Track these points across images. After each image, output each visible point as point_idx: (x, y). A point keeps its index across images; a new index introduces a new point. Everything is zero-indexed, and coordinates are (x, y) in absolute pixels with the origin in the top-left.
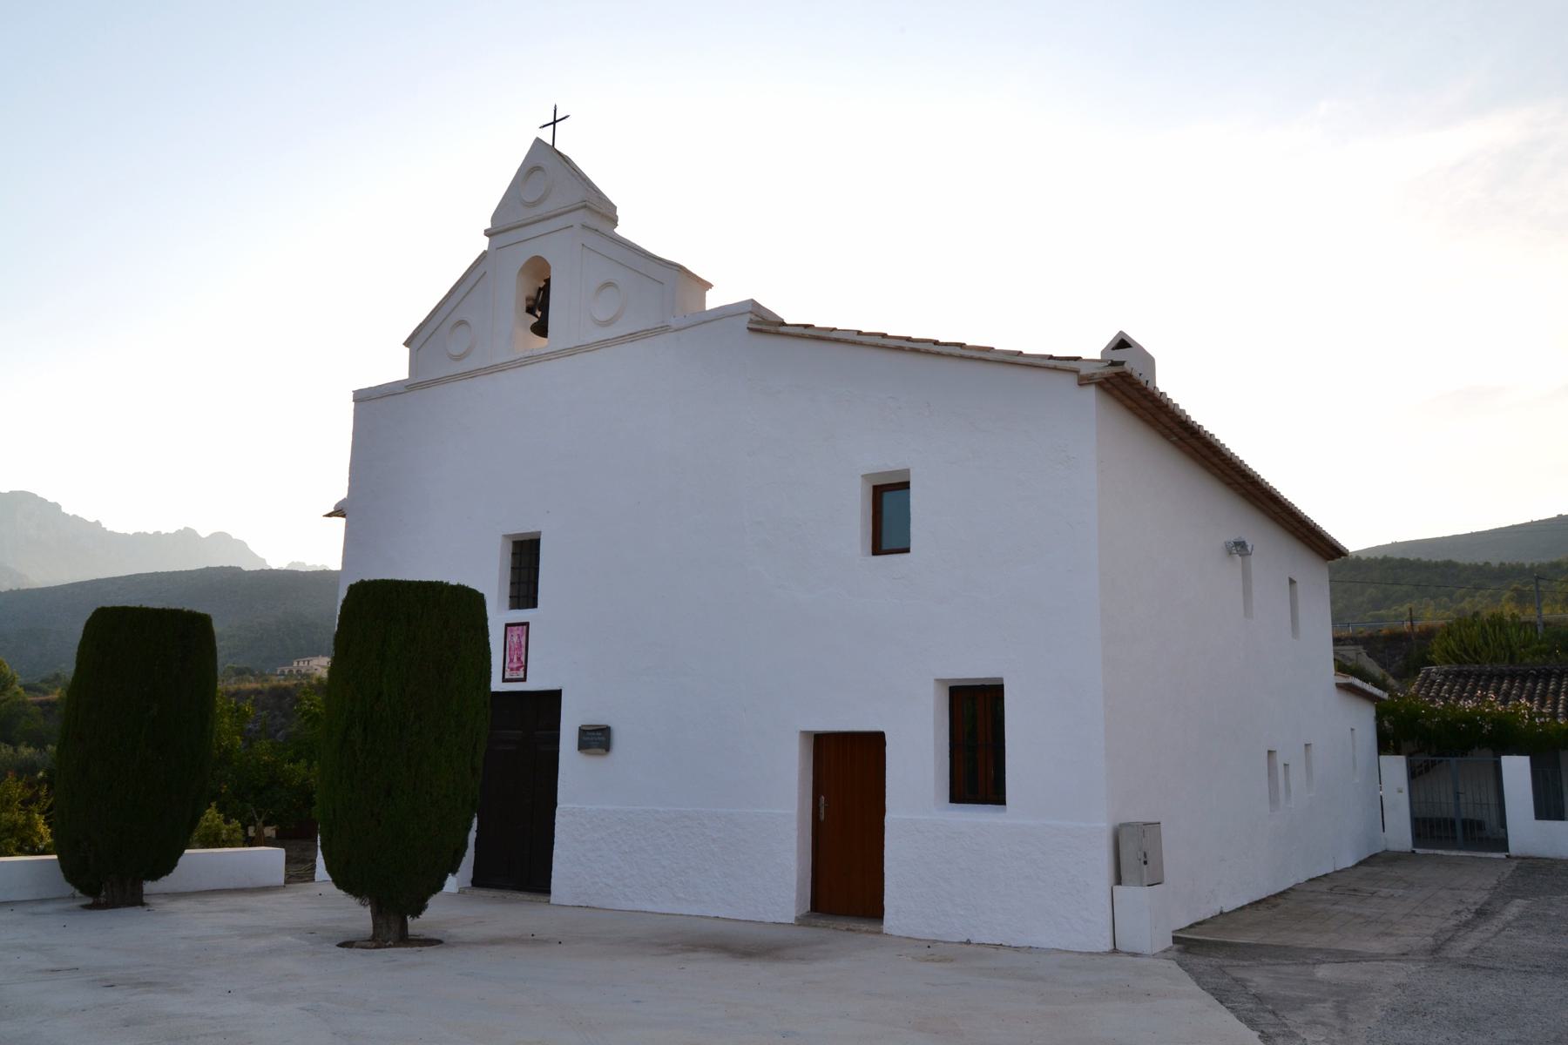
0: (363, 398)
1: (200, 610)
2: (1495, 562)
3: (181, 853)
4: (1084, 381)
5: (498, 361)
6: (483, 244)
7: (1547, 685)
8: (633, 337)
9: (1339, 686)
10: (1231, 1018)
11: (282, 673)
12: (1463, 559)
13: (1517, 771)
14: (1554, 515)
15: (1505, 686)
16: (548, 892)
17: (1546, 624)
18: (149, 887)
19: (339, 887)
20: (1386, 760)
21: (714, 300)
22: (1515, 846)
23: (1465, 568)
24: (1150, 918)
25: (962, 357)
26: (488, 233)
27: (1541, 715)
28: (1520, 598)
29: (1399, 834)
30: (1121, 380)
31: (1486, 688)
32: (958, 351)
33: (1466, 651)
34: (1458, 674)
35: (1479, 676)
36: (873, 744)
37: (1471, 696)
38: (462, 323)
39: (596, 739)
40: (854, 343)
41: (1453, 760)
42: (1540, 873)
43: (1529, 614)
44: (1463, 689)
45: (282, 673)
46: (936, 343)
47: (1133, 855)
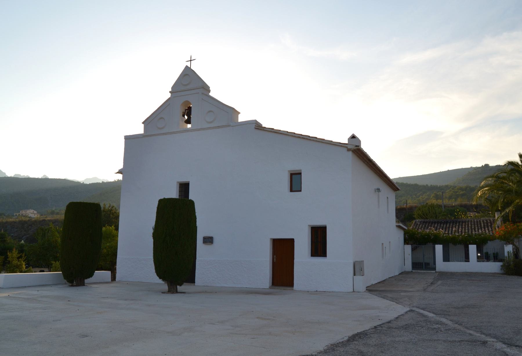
0: (128, 138)
1: (96, 202)
2: (429, 185)
3: (94, 272)
4: (349, 150)
5: (175, 131)
6: (169, 95)
7: (446, 225)
8: (219, 127)
9: (397, 226)
10: (388, 301)
11: (16, 215)
12: (420, 183)
13: (439, 248)
14: (469, 167)
15: (436, 225)
16: (194, 283)
17: (445, 206)
18: (86, 281)
19: (160, 278)
20: (406, 246)
21: (242, 118)
22: (438, 269)
23: (421, 186)
24: (361, 283)
25: (316, 141)
26: (170, 92)
27: (445, 234)
28: (437, 197)
29: (408, 267)
30: (355, 149)
31: (431, 226)
32: (315, 139)
33: (424, 215)
34: (424, 222)
35: (429, 222)
36: (291, 242)
37: (427, 229)
38: (161, 118)
39: (209, 240)
40: (286, 135)
41: (423, 246)
42: (444, 275)
43: (440, 202)
44: (425, 226)
45: (16, 215)
46: (309, 136)
47: (358, 268)
